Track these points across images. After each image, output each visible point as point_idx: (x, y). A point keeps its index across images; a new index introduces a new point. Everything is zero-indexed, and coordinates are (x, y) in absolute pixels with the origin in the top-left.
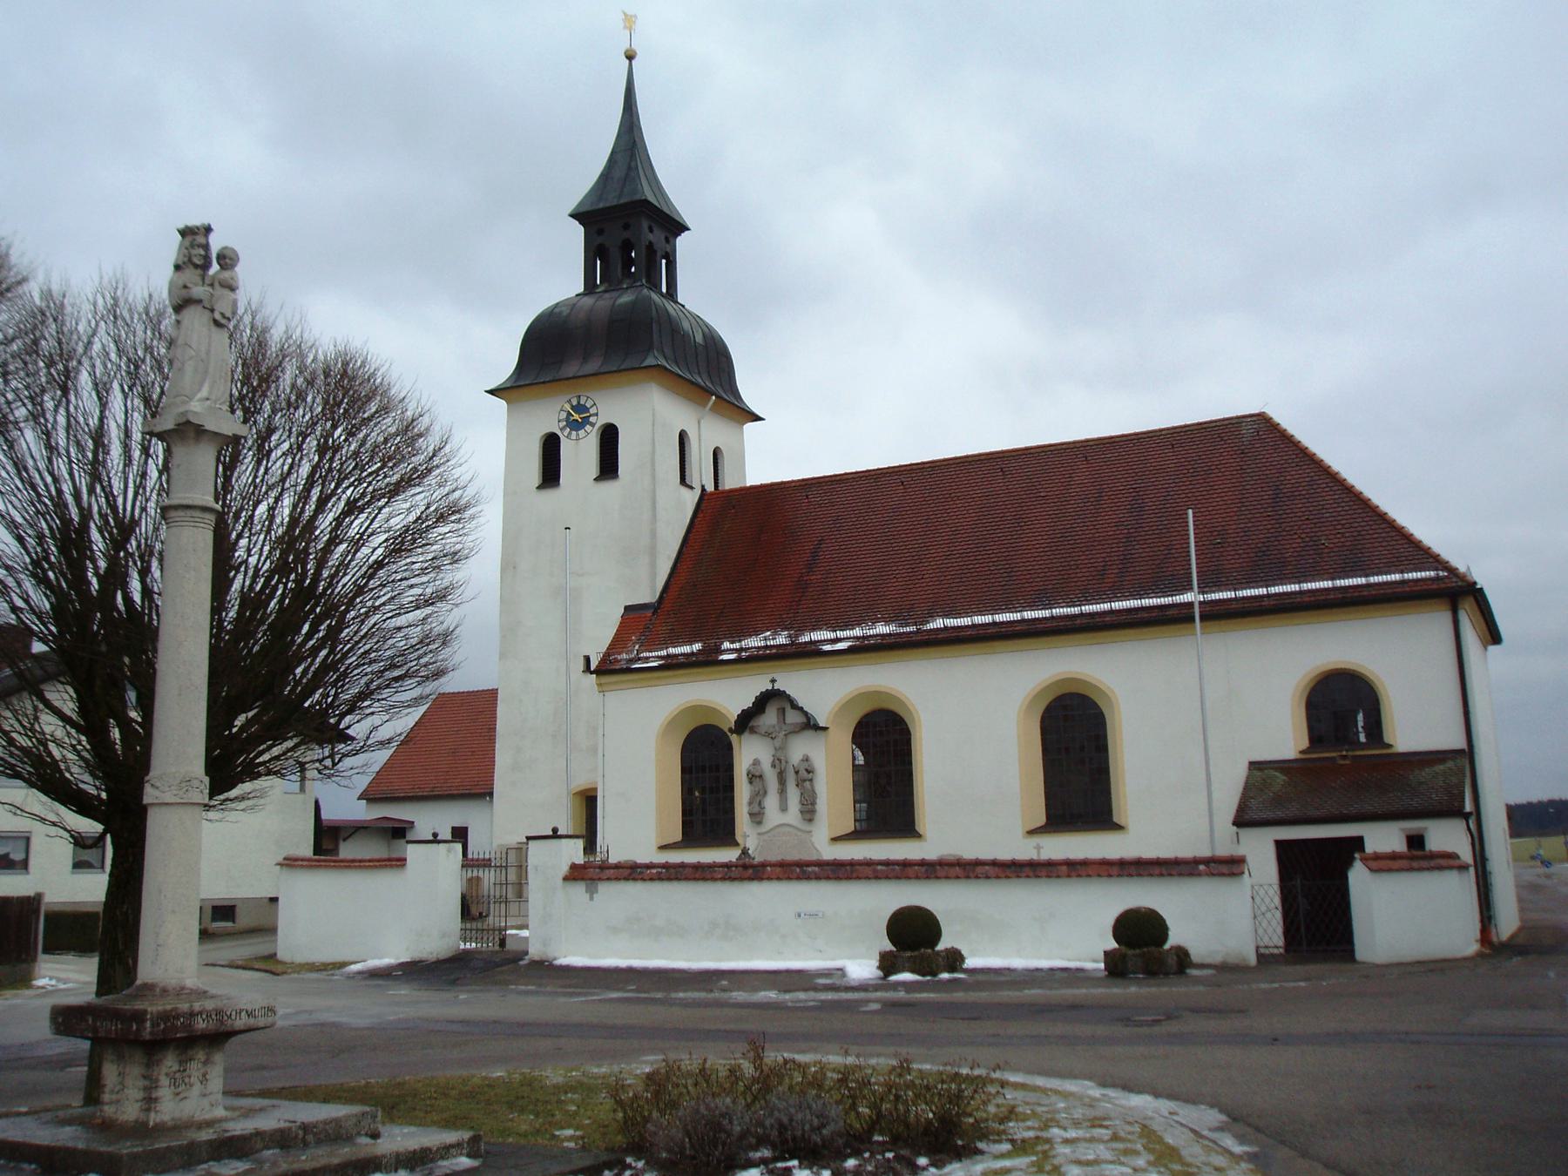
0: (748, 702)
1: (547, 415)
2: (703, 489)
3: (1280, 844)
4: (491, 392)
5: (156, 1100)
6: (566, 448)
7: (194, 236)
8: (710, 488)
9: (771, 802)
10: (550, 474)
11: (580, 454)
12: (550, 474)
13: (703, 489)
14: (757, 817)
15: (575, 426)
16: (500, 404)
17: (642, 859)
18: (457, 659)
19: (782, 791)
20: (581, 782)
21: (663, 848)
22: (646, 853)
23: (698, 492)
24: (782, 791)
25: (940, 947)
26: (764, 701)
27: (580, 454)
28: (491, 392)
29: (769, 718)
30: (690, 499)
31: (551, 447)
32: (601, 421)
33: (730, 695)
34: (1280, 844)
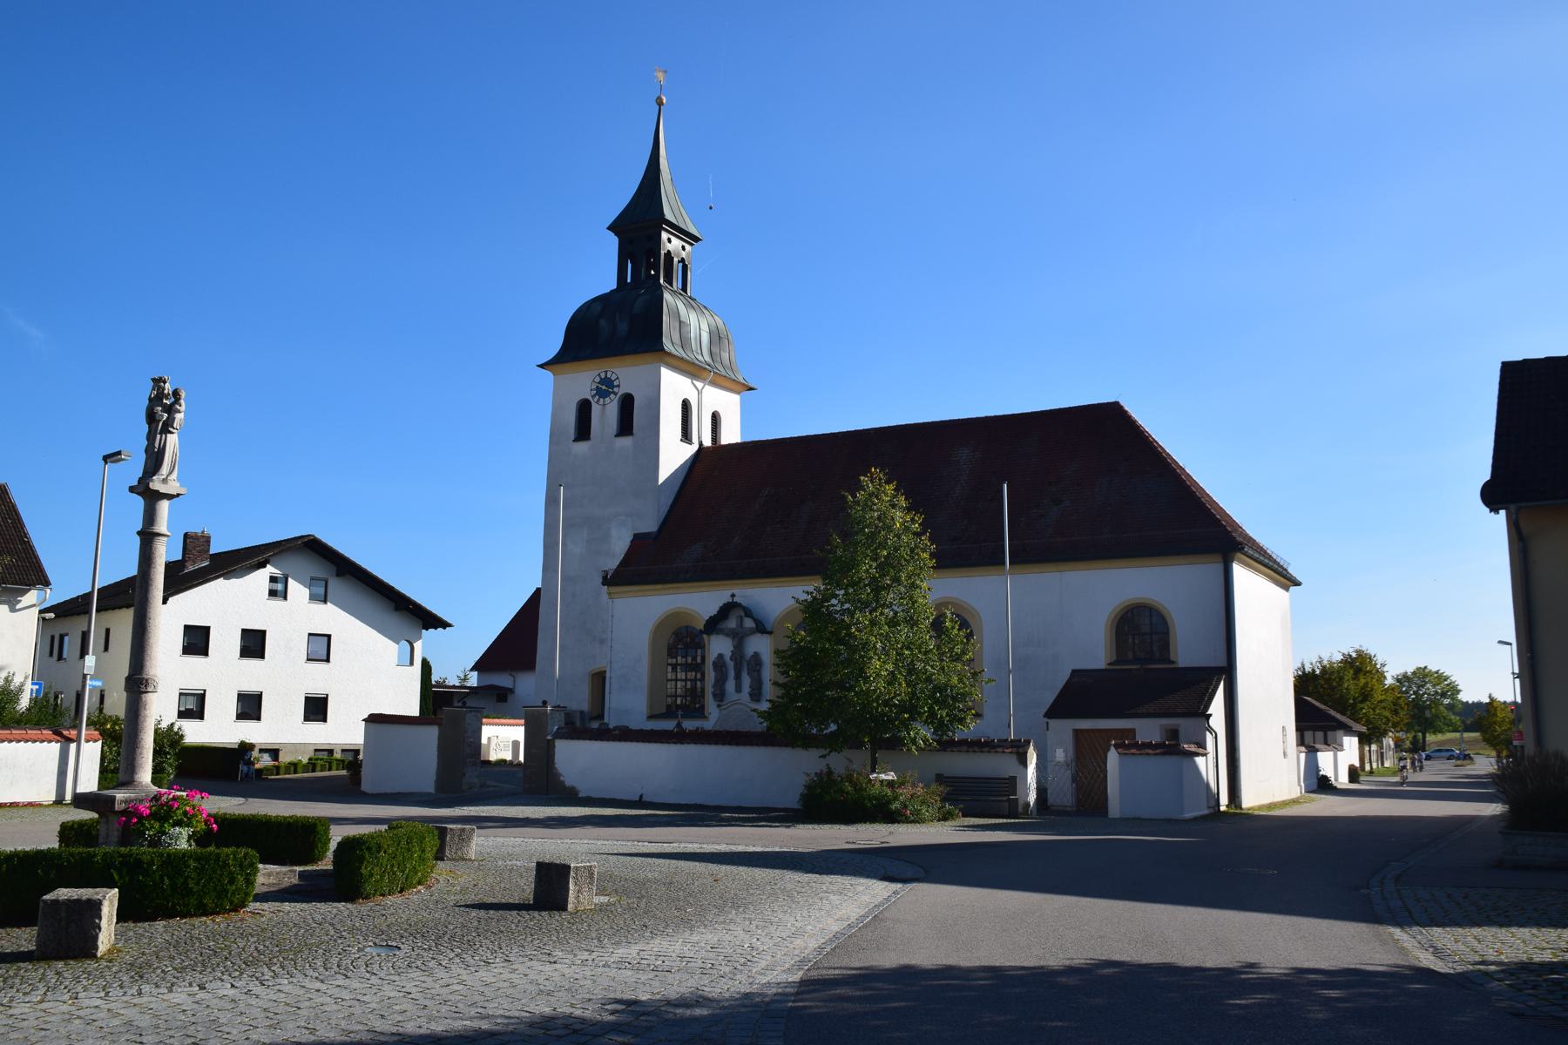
0: (713, 610)
1: (583, 380)
2: (701, 444)
3: (1077, 732)
4: (541, 366)
5: (1398, 680)
6: (596, 410)
7: (1297, 584)
8: (707, 442)
9: (730, 685)
10: (583, 430)
11: (605, 415)
12: (583, 430)
13: (701, 444)
14: (720, 695)
15: (602, 394)
16: (547, 375)
17: (633, 726)
18: (793, 602)
19: (738, 677)
20: (596, 667)
21: (651, 717)
22: (639, 721)
23: (695, 447)
24: (738, 677)
25: (1389, 681)
26: (726, 610)
27: (605, 415)
28: (541, 366)
29: (732, 623)
30: (690, 450)
31: (584, 409)
32: (622, 391)
33: (701, 601)
34: (1077, 732)
